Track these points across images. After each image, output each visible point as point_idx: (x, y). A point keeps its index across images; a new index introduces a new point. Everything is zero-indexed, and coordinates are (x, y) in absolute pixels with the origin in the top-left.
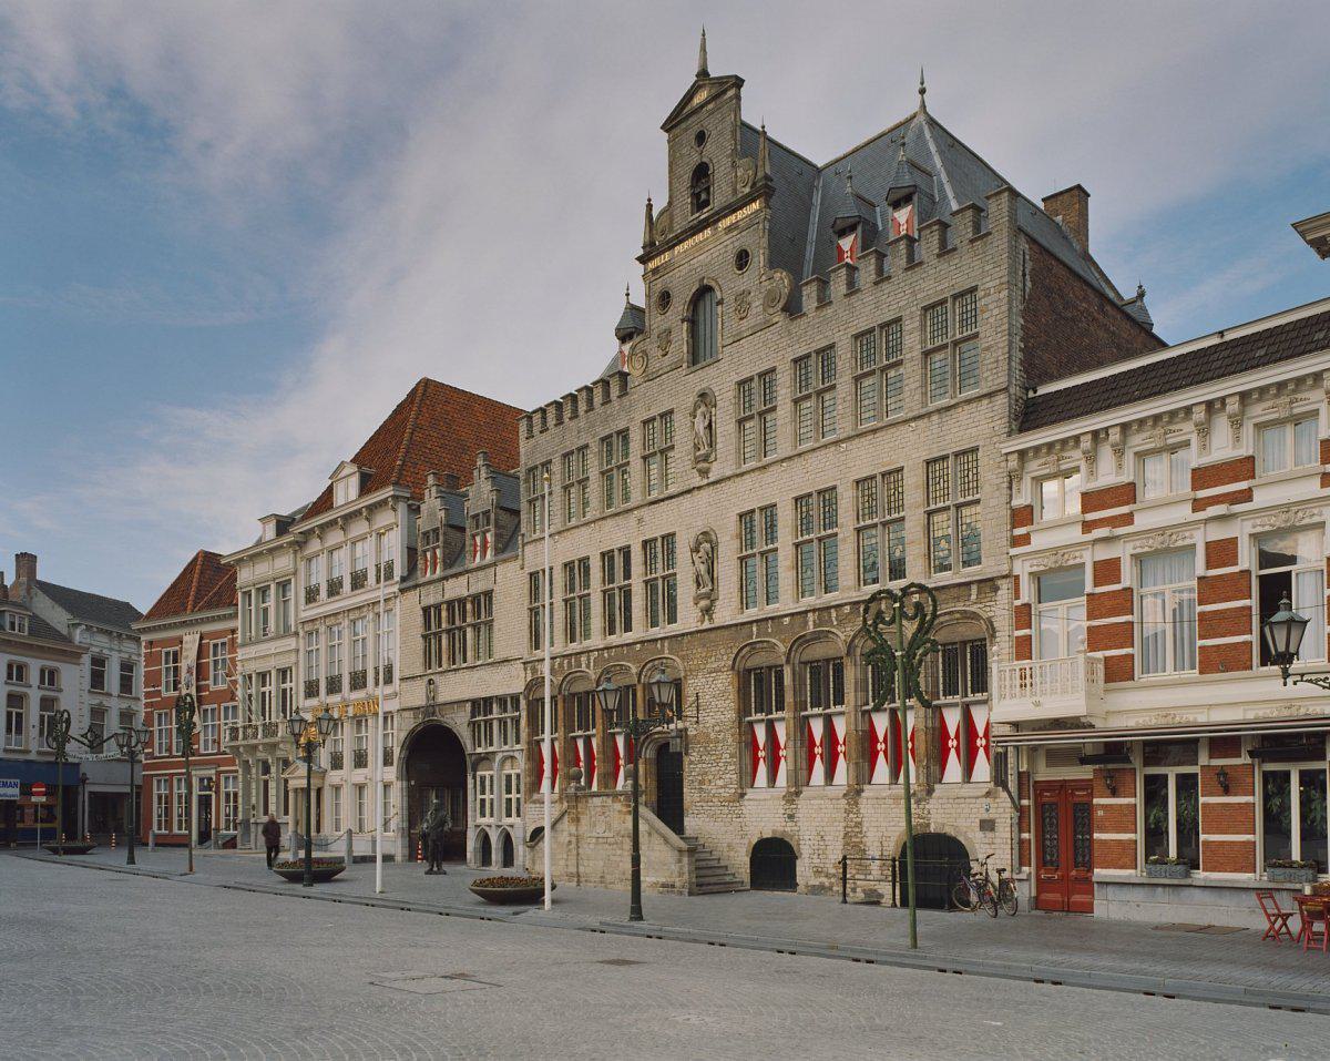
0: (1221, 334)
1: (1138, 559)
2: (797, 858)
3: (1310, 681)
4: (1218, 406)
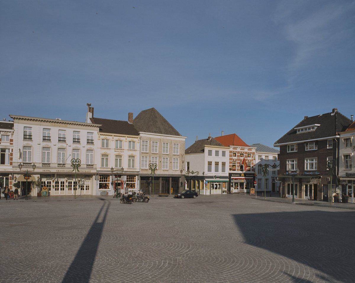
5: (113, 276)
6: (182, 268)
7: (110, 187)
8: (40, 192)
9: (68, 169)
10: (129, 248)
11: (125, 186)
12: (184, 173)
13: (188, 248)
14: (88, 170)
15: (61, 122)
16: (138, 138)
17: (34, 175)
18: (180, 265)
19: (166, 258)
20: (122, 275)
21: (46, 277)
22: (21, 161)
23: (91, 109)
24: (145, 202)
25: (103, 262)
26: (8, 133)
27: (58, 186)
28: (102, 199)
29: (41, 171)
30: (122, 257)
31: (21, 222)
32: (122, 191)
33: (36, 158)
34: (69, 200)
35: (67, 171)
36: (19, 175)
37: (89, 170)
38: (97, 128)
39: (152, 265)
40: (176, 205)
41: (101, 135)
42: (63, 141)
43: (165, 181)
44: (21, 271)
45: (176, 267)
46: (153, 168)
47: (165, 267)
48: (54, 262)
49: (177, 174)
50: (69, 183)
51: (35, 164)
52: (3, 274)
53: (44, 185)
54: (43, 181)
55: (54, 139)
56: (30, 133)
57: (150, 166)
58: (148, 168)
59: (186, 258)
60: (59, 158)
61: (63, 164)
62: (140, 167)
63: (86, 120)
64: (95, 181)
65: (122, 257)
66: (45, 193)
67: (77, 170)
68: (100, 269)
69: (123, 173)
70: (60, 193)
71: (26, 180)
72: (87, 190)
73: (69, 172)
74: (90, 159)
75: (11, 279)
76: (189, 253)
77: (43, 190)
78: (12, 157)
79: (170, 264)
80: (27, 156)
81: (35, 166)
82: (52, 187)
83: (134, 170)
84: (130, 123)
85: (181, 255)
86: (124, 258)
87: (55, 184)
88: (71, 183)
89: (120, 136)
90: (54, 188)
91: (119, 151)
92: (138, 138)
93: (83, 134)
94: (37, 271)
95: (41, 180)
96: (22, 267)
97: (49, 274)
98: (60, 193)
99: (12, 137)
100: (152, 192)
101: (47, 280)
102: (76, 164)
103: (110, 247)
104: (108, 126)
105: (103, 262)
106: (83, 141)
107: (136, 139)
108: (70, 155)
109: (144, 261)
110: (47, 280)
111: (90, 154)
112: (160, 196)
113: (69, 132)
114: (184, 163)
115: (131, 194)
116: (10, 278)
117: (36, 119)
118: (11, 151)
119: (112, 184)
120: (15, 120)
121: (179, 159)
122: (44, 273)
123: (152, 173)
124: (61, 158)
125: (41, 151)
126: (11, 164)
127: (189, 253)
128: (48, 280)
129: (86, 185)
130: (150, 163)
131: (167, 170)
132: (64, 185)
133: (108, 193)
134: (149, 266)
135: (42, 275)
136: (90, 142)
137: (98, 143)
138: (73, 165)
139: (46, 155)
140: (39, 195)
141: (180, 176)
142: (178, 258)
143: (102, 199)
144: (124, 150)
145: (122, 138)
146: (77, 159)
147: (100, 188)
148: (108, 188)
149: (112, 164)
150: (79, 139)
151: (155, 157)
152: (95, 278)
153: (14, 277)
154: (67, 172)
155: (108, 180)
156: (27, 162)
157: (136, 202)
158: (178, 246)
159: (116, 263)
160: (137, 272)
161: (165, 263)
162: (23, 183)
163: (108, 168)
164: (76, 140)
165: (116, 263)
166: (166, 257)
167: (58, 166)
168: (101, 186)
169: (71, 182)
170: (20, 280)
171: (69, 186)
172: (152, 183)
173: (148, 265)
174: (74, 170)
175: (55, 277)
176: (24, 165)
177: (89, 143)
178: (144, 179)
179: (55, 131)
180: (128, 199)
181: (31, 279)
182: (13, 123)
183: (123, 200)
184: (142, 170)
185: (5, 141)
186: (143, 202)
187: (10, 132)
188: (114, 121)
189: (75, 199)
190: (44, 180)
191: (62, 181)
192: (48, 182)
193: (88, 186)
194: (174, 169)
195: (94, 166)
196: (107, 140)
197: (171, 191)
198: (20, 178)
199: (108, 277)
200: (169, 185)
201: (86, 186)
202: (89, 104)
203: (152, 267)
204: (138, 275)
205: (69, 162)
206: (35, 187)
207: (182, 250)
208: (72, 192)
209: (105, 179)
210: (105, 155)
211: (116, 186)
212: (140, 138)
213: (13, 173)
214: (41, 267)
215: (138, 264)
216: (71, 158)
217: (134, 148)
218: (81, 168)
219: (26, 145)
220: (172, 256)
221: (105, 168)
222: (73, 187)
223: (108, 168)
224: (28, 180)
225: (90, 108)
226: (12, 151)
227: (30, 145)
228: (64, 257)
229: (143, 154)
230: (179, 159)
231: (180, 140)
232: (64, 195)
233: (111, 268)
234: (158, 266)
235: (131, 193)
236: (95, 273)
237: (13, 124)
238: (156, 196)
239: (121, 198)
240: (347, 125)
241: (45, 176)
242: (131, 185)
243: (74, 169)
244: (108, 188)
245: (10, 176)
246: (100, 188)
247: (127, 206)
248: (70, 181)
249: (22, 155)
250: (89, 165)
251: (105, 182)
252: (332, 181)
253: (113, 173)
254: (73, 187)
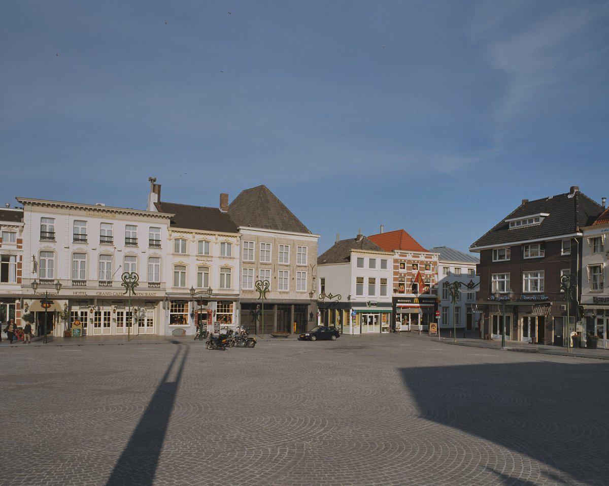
5: (194, 474)
6: (313, 460)
7: (188, 322)
8: (69, 329)
9: (116, 290)
10: (222, 426)
11: (214, 319)
12: (315, 297)
13: (323, 426)
14: (150, 292)
15: (104, 210)
16: (236, 237)
17: (58, 301)
18: (310, 455)
19: (284, 444)
20: (209, 473)
21: (78, 476)
22: (36, 276)
23: (157, 187)
24: (249, 347)
25: (177, 450)
26: (14, 228)
27: (100, 320)
28: (176, 342)
29: (70, 293)
30: (210, 441)
31: (37, 382)
32: (210, 329)
33: (63, 271)
34: (119, 343)
35: (115, 294)
36: (33, 301)
37: (153, 292)
38: (166, 220)
39: (261, 455)
40: (301, 352)
41: (173, 231)
42: (108, 242)
43: (282, 311)
44: (36, 465)
45: (302, 459)
46: (263, 288)
47: (284, 458)
48: (92, 449)
49: (303, 299)
50: (118, 315)
51: (60, 282)
52: (6, 471)
53: (76, 318)
54: (74, 311)
55: (93, 238)
56: (52, 228)
57: (257, 285)
58: (253, 288)
59: (319, 443)
60: (100, 272)
61: (109, 282)
62: (241, 287)
63: (148, 206)
64: (162, 311)
65: (210, 441)
66: (77, 331)
67: (131, 292)
68: (172, 461)
69: (211, 297)
70: (102, 331)
71: (44, 310)
72: (150, 327)
73: (119, 296)
74: (154, 273)
75: (19, 479)
76: (324, 434)
77: (74, 327)
78: (20, 269)
79: (291, 453)
80: (47, 268)
81: (61, 285)
82: (88, 321)
83: (231, 293)
84: (223, 212)
85: (310, 438)
86: (213, 443)
87: (94, 317)
88: (122, 315)
89: (205, 234)
90: (92, 323)
91: (205, 259)
92: (236, 237)
93: (143, 229)
94: (63, 465)
95: (70, 309)
96: (38, 459)
97: (83, 470)
98: (102, 331)
99: (20, 235)
100: (260, 329)
101: (80, 481)
102: (130, 282)
103: (189, 424)
104: (185, 217)
105: (177, 450)
106: (143, 242)
107: (233, 240)
108: (120, 266)
109: (247, 447)
110: (80, 481)
111: (154, 264)
112: (275, 337)
113: (119, 227)
114: (315, 280)
116: (17, 477)
117: (61, 205)
118: (18, 260)
119: (192, 315)
120: (26, 207)
121: (307, 272)
122: (76, 468)
123: (261, 297)
124: (105, 271)
125: (70, 260)
126: (19, 281)
127: (324, 434)
128: (82, 480)
129: (148, 318)
130: (257, 279)
131: (287, 293)
132: (109, 318)
133: (185, 331)
134: (256, 457)
135: (73, 471)
136: (154, 243)
137: (168, 245)
138: (126, 283)
139: (79, 267)
140: (67, 334)
141: (309, 302)
142: (305, 443)
143: (176, 342)
144: (212, 257)
145: (209, 238)
146: (132, 273)
147: (171, 323)
148: (186, 323)
149: (192, 282)
150: (136, 239)
151: (265, 270)
152: (162, 478)
153: (25, 475)
154: (115, 296)
155: (185, 308)
156: (47, 278)
157: (233, 346)
158: (305, 423)
159: (200, 451)
160: (235, 466)
161: (283, 451)
162: (40, 314)
163: (186, 289)
164: (131, 241)
165: (200, 451)
166: (285, 441)
167: (100, 286)
168: (173, 320)
169: (122, 313)
170: (35, 481)
171: (118, 320)
172: (261, 315)
173: (254, 455)
174: (126, 292)
175: (95, 476)
176: (42, 283)
177: (153, 245)
178: (247, 307)
179: (94, 226)
180: (220, 342)
181: (54, 480)
182: (22, 210)
183: (212, 343)
184: (244, 291)
185: (9, 242)
186: (245, 346)
187: (18, 226)
188: (196, 207)
189: (129, 341)
190: (75, 309)
191: (107, 311)
192: (82, 313)
193: (152, 320)
194: (298, 291)
195: (161, 286)
196: (184, 240)
197: (294, 328)
198: (35, 306)
199: (186, 475)
200: (289, 317)
201: (148, 320)
202: (153, 178)
203: (261, 459)
204: (237, 472)
205: (118, 279)
206: (60, 321)
207: (312, 429)
208: (124, 330)
209: (179, 307)
210: (180, 267)
211: (199, 319)
212: (240, 237)
213: (22, 298)
214: (70, 458)
215: (237, 453)
216: (121, 271)
217: (229, 253)
218: (138, 288)
219: (44, 249)
220: (295, 439)
221: (180, 288)
222: (124, 322)
223: (186, 289)
224: (49, 310)
225: (154, 185)
226: (21, 260)
227: (51, 250)
228: (110, 442)
229: (246, 265)
230: (306, 274)
231: (309, 240)
232: (111, 334)
233: (191, 460)
234: (272, 456)
235: (224, 332)
236: (164, 468)
237: (23, 212)
238: (267, 337)
239: (208, 339)
241: (77, 302)
242: (224, 317)
243: (127, 290)
244: (186, 323)
245: (17, 301)
246: (171, 323)
247: (218, 354)
248: (120, 311)
249: (38, 266)
250: (153, 284)
251: (179, 313)
253: (194, 296)
254: (124, 322)
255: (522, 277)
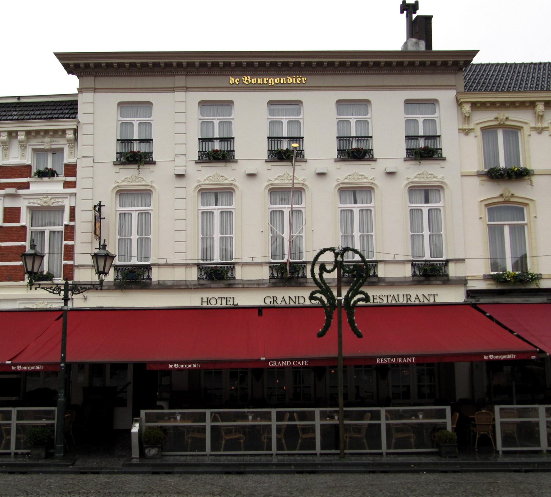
0: (19, 98)
1: (32, 210)
2: (126, 400)
3: (43, 288)
4: (14, 135)
41: (474, 105)
78: (70, 243)
115: (133, 456)
240: (404, 2)
252: (530, 422)
255: (274, 368)
